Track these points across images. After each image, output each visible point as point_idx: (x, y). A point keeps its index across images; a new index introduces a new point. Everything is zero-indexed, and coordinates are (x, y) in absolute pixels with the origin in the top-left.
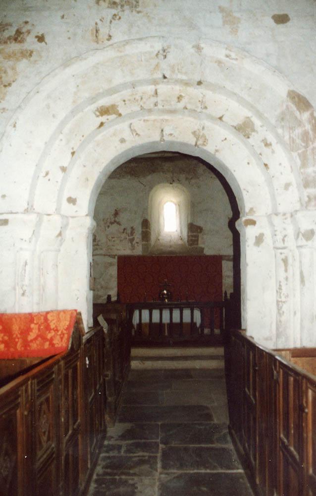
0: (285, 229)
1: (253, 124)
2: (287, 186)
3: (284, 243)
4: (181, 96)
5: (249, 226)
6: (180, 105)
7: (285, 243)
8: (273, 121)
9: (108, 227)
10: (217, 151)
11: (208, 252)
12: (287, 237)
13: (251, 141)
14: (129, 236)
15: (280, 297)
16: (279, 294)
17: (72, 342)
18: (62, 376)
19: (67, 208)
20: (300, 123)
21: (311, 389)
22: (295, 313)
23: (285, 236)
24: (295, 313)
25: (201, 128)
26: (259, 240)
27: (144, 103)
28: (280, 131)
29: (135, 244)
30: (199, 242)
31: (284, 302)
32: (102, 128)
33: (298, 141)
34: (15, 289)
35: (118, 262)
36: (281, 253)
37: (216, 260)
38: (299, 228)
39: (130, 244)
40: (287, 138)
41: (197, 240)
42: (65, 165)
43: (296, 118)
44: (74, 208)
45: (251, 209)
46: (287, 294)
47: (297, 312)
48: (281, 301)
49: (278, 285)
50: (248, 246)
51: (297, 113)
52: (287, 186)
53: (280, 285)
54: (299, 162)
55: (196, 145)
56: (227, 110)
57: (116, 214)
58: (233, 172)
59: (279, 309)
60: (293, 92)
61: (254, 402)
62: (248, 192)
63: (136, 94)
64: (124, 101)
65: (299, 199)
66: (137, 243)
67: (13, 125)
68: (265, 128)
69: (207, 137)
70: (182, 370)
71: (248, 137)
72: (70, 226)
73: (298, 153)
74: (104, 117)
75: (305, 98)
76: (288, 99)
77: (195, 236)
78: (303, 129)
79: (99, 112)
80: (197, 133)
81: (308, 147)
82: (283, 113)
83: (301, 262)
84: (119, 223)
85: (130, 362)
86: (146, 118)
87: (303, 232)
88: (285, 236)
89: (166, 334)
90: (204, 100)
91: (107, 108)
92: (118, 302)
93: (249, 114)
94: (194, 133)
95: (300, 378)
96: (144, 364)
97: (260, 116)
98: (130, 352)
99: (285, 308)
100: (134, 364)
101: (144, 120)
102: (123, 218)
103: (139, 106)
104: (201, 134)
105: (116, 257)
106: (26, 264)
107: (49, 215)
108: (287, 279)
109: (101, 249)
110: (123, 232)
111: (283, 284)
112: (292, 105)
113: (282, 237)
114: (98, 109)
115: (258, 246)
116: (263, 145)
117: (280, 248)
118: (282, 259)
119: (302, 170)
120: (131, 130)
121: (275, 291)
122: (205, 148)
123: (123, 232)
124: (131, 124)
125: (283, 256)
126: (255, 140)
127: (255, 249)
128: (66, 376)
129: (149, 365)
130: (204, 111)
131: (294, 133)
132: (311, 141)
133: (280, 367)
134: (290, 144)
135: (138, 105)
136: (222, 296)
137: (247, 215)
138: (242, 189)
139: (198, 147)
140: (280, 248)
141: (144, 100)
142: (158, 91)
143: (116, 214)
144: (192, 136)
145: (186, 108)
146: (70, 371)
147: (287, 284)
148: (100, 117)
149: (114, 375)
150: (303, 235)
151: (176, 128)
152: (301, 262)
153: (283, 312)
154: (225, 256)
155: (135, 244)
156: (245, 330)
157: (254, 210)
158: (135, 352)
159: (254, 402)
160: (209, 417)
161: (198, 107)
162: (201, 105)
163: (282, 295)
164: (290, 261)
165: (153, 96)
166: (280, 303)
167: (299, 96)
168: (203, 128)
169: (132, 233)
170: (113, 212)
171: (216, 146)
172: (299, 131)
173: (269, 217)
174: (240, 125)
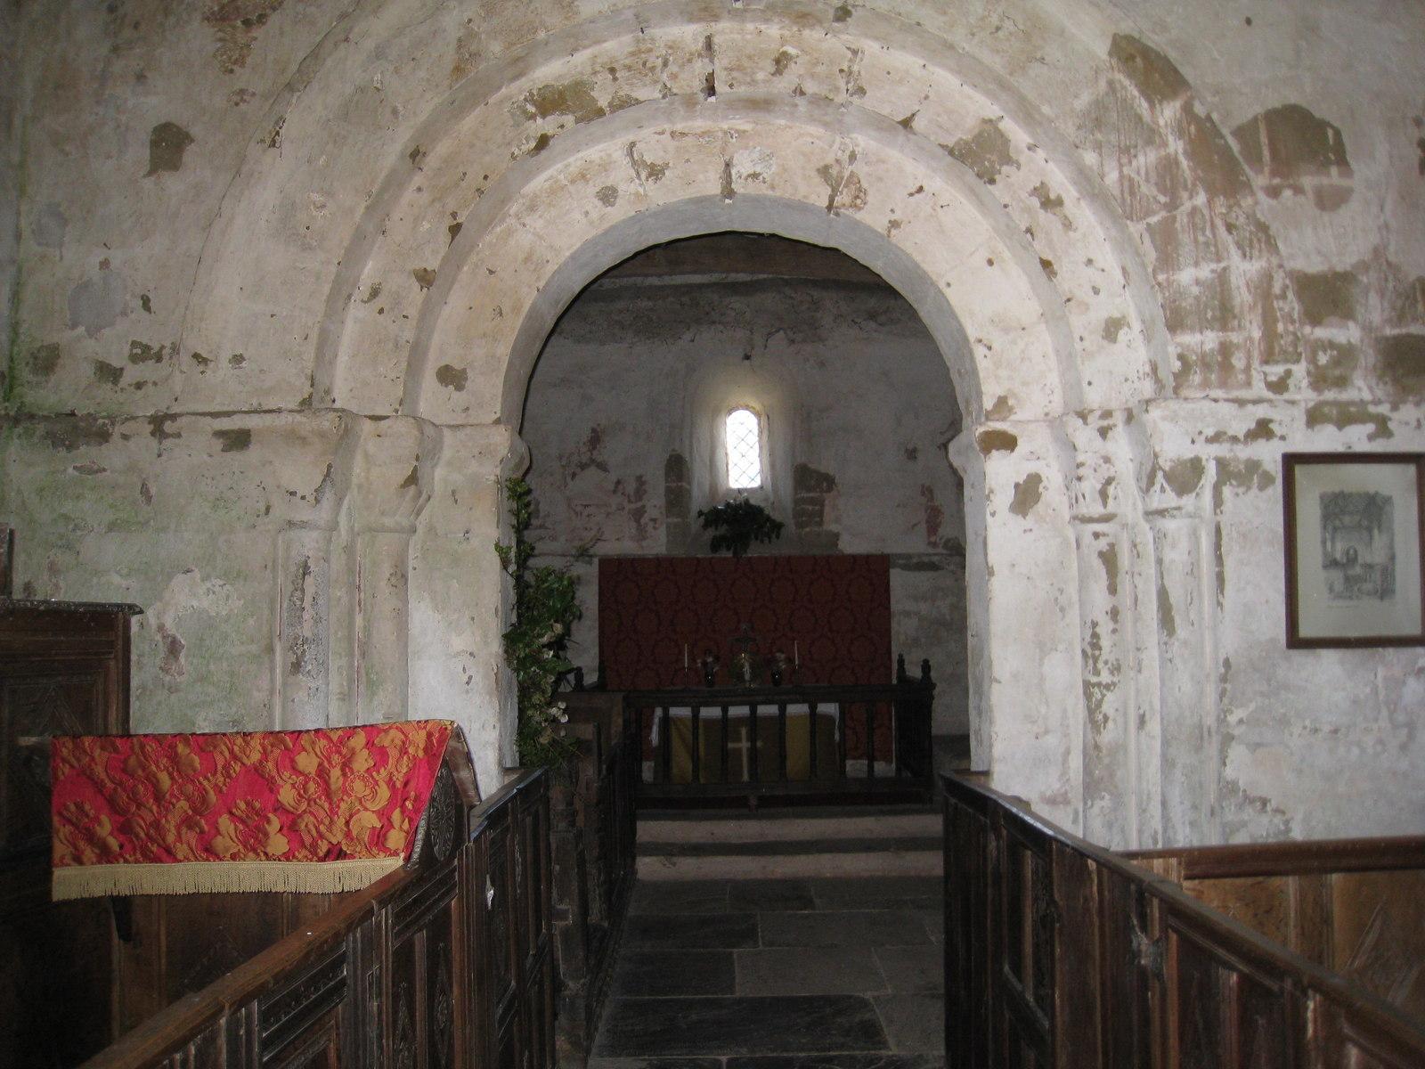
0: (1107, 460)
1: (1006, 142)
2: (1112, 329)
3: (1105, 504)
4: (784, 54)
5: (994, 453)
6: (784, 84)
7: (1110, 501)
8: (1069, 129)
9: (574, 475)
10: (894, 224)
11: (850, 545)
12: (1114, 484)
13: (998, 191)
14: (629, 501)
15: (1097, 672)
16: (1091, 662)
17: (428, 834)
18: (382, 966)
19: (433, 399)
20: (1151, 136)
21: (1356, 1044)
22: (1142, 721)
23: (1109, 481)
24: (1142, 721)
25: (845, 157)
26: (1027, 495)
27: (674, 77)
28: (1090, 158)
29: (646, 524)
30: (826, 518)
31: (1107, 687)
32: (544, 153)
33: (1147, 190)
34: (270, 649)
35: (601, 573)
36: (1096, 535)
37: (875, 569)
38: (1156, 456)
39: (633, 524)
40: (1112, 177)
41: (821, 514)
42: (433, 264)
43: (1139, 118)
44: (459, 398)
45: (1002, 402)
46: (1117, 660)
47: (1147, 717)
48: (1099, 685)
49: (1089, 632)
50: (993, 514)
51: (1143, 106)
52: (1112, 329)
53: (1095, 635)
54: (1151, 255)
55: (830, 207)
56: (926, 97)
57: (595, 439)
58: (942, 285)
59: (1093, 709)
60: (1129, 39)
61: (1047, 1024)
62: (990, 348)
63: (650, 50)
64: (612, 70)
65: (1147, 369)
66: (654, 520)
67: (268, 141)
68: (1041, 154)
69: (865, 185)
70: (783, 882)
71: (992, 181)
72: (447, 453)
73: (1148, 224)
74: (549, 118)
75: (1166, 59)
76: (1114, 61)
77: (812, 501)
78: (1163, 153)
79: (534, 103)
80: (834, 171)
81: (1176, 208)
82: (1098, 104)
83: (1160, 562)
84: (603, 467)
85: (634, 859)
86: (679, 127)
87: (1167, 469)
88: (1109, 481)
89: (746, 777)
90: (855, 68)
91: (561, 93)
92: (601, 686)
93: (992, 110)
94: (824, 171)
95: (1288, 984)
96: (674, 864)
97: (1027, 114)
98: (633, 831)
99: (1110, 704)
100: (647, 867)
101: (673, 134)
102: (614, 451)
103: (659, 86)
104: (846, 174)
105: (596, 561)
106: (306, 570)
107: (377, 418)
108: (1114, 614)
109: (554, 539)
110: (614, 492)
111: (1105, 628)
112: (1127, 82)
113: (1099, 486)
114: (531, 94)
115: (1024, 515)
116: (1035, 202)
117: (1091, 520)
118: (1101, 554)
119: (1161, 277)
120: (634, 163)
121: (1079, 652)
122: (859, 216)
123: (614, 492)
124: (633, 145)
125: (1102, 544)
126: (1015, 184)
127: (1018, 523)
128: (404, 957)
129: (689, 868)
130: (856, 100)
131: (1134, 163)
132: (1185, 188)
133: (1165, 928)
134: (1123, 199)
135: (656, 82)
136: (889, 668)
137: (987, 419)
138: (972, 340)
139: (837, 214)
140: (1091, 520)
141: (673, 68)
142: (716, 40)
143: (595, 439)
144: (817, 180)
145: (802, 93)
146: (420, 939)
147: (1114, 631)
148: (539, 120)
149: (584, 910)
150: (1167, 477)
151: (771, 155)
152: (1160, 562)
153: (1106, 718)
154: (900, 556)
155: (646, 524)
156: (986, 774)
157: (1011, 402)
158: (647, 830)
159: (1047, 1024)
160: (871, 1033)
161: (837, 89)
162: (848, 83)
163: (1100, 665)
164: (1125, 560)
165: (700, 55)
166: (1096, 690)
167: (1146, 52)
168: (853, 157)
169: (640, 493)
170: (586, 435)
171: (892, 211)
172: (1147, 159)
173: (1054, 423)
174: (966, 143)
